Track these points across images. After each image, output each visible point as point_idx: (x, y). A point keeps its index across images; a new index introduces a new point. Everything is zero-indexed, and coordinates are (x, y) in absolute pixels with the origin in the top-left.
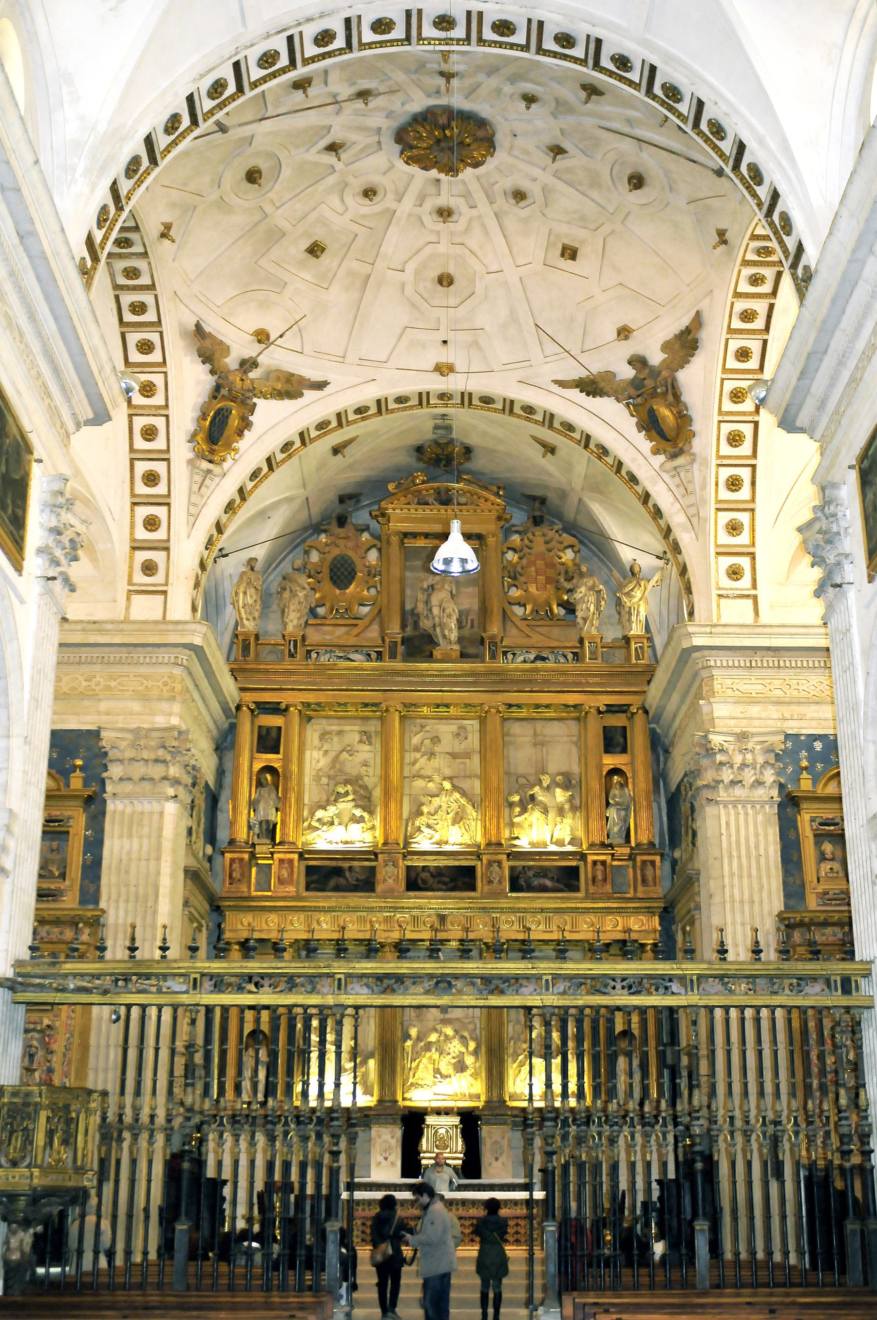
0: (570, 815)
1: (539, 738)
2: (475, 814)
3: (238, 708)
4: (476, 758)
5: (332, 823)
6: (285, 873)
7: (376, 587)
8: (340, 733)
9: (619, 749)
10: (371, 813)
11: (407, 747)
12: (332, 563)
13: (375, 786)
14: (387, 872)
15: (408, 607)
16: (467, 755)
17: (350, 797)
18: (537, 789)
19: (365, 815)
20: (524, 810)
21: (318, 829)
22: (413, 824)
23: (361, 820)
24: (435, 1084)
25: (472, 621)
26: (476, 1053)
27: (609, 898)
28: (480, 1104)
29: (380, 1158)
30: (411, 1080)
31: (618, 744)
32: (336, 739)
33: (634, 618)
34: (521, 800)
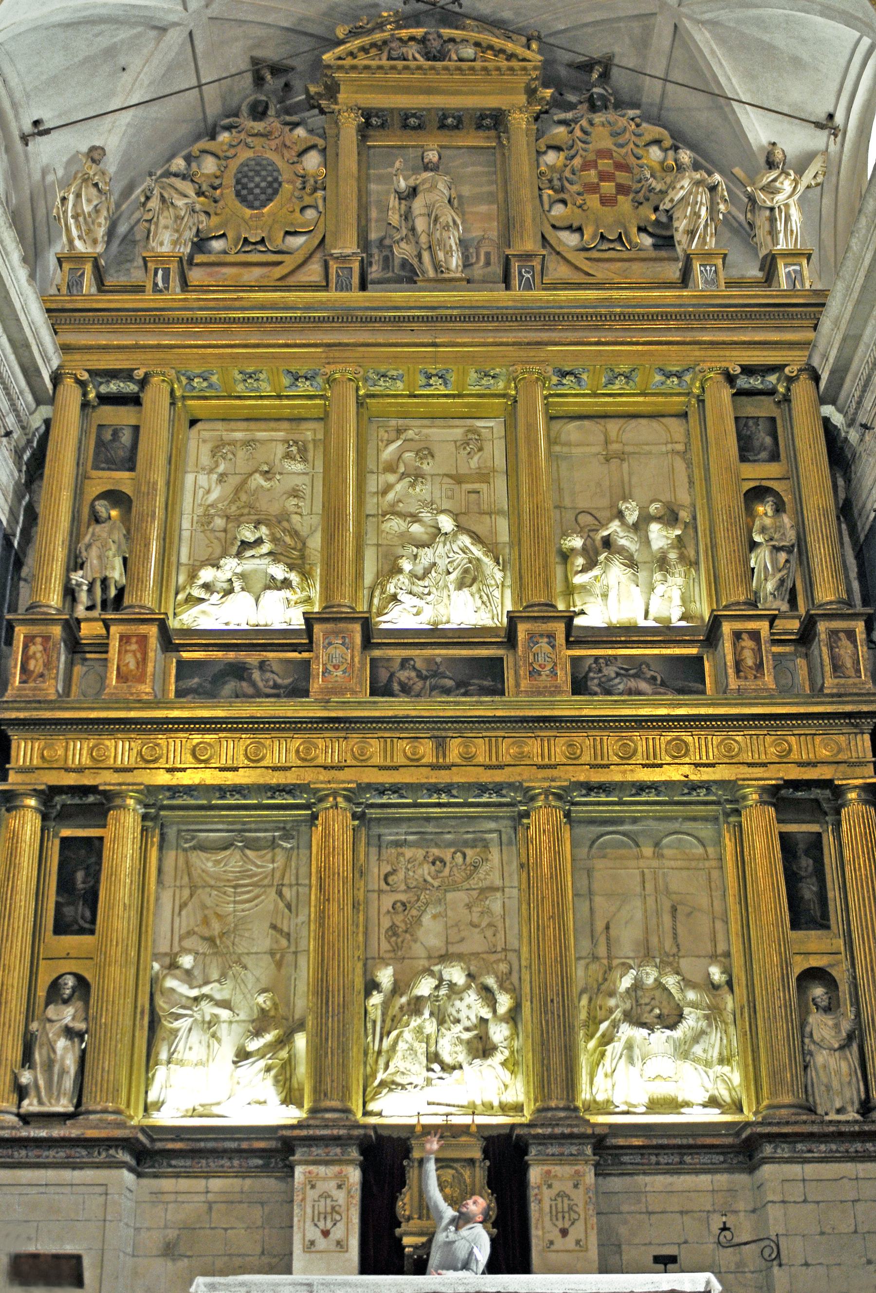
0: (680, 569)
1: (615, 447)
2: (499, 575)
3: (57, 378)
4: (500, 483)
5: (229, 591)
6: (131, 661)
7: (316, 207)
8: (247, 443)
9: (764, 455)
10: (305, 575)
11: (371, 465)
12: (239, 171)
13: (313, 532)
14: (330, 658)
15: (373, 236)
16: (484, 476)
17: (266, 548)
18: (615, 526)
19: (294, 577)
20: (591, 564)
21: (202, 600)
22: (383, 592)
23: (286, 584)
24: (429, 1082)
25: (488, 255)
26: (513, 1016)
27: (770, 699)
28: (526, 1117)
29: (313, 1233)
30: (381, 1076)
31: (763, 448)
32: (241, 454)
33: (780, 226)
34: (584, 548)
